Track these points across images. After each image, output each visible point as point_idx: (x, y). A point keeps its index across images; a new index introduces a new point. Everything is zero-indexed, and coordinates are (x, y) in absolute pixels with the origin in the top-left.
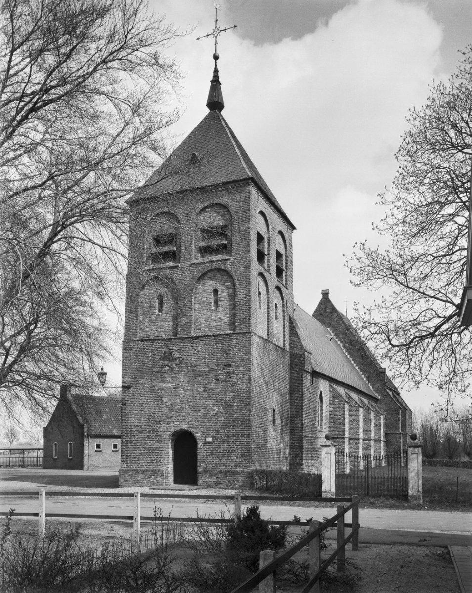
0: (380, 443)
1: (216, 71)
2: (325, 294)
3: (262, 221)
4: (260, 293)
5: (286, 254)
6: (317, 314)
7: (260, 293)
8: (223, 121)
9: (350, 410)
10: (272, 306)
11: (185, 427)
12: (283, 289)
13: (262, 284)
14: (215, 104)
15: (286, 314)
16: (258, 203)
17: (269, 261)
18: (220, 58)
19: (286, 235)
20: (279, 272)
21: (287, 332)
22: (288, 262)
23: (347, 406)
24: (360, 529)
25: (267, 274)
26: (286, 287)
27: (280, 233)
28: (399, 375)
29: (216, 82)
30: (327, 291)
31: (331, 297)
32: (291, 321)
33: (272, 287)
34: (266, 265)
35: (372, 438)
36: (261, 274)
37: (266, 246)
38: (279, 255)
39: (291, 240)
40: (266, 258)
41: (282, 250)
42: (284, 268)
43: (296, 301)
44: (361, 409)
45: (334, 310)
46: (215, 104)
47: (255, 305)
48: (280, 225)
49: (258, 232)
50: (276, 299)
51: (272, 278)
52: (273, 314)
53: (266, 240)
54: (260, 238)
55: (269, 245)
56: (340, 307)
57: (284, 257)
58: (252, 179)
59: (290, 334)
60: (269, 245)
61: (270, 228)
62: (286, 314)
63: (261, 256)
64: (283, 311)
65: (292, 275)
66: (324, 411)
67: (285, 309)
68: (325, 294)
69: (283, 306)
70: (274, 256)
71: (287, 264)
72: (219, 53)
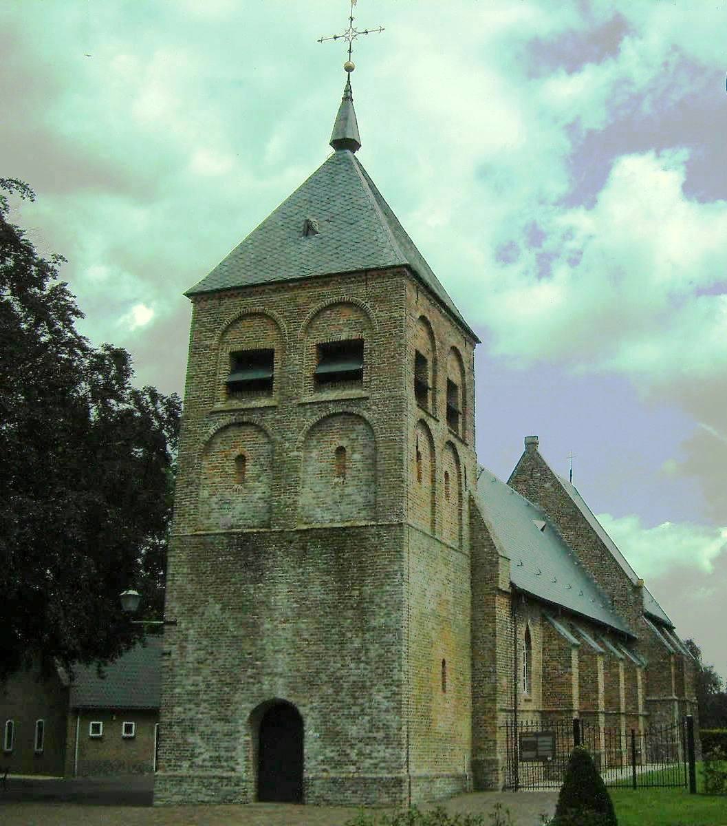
0: (638, 719)
1: (348, 90)
2: (532, 444)
3: (423, 334)
4: (418, 454)
5: (464, 385)
6: (514, 481)
7: (418, 454)
8: (357, 166)
9: (619, 703)
10: (440, 476)
11: (282, 694)
12: (458, 445)
13: (423, 438)
14: (345, 143)
15: (464, 488)
16: (417, 305)
17: (434, 400)
18: (355, 70)
19: (463, 354)
20: (452, 415)
21: (466, 519)
22: (468, 399)
23: (574, 653)
24: (349, 152)
25: (431, 423)
26: (463, 442)
27: (454, 349)
28: (214, 511)
29: (348, 98)
30: (535, 440)
31: (540, 449)
32: (475, 514)
33: (438, 444)
34: (430, 404)
35: (623, 710)
36: (422, 423)
37: (430, 373)
38: (451, 387)
39: (472, 361)
40: (430, 393)
41: (456, 378)
42: (460, 409)
43: (482, 462)
44: (621, 664)
45: (546, 472)
46: (345, 143)
47: (410, 475)
48: (454, 339)
49: (417, 352)
50: (445, 461)
51: (440, 428)
52: (440, 487)
53: (430, 364)
54: (420, 360)
55: (435, 372)
56: (559, 469)
57: (460, 391)
58: (406, 266)
59: (471, 517)
60: (435, 372)
61: (437, 343)
62: (464, 488)
63: (421, 390)
64: (460, 485)
65: (473, 421)
66: (533, 662)
67: (463, 480)
68: (532, 444)
69: (459, 476)
70: (442, 387)
71: (465, 403)
72: (355, 60)
